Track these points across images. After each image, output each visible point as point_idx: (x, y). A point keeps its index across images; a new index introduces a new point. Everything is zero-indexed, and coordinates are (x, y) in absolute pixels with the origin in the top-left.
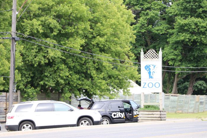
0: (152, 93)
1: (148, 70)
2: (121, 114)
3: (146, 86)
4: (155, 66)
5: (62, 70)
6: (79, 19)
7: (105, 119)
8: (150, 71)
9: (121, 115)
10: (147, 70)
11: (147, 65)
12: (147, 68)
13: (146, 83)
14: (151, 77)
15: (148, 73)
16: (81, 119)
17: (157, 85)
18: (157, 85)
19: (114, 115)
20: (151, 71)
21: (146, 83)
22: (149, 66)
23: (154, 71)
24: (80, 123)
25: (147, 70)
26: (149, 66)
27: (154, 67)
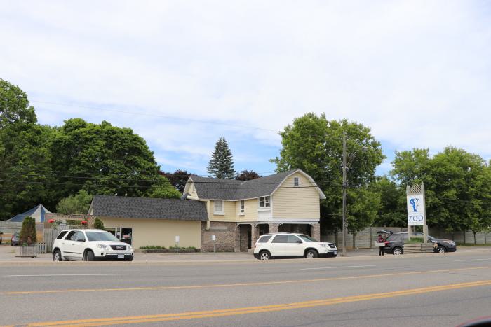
5: (443, 212)
6: (455, 176)
14: (415, 211)
16: (308, 251)
18: (421, 218)
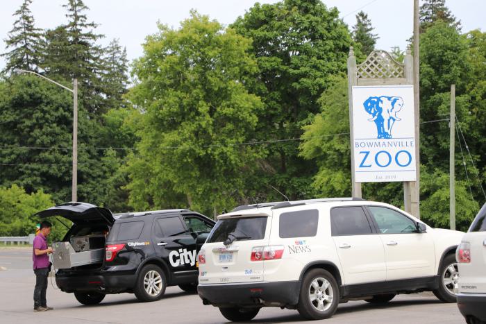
0: (125, 51)
1: (375, 112)
2: (190, 253)
3: (370, 160)
4: (395, 100)
7: (160, 281)
8: (380, 115)
9: (189, 258)
10: (370, 113)
11: (371, 98)
12: (371, 107)
13: (368, 153)
14: (383, 134)
15: (376, 121)
17: (403, 159)
18: (403, 159)
19: (175, 258)
20: (385, 115)
21: (368, 153)
22: (376, 100)
23: (392, 114)
24: (152, 297)
25: (372, 112)
26: (379, 99)
27: (393, 104)
